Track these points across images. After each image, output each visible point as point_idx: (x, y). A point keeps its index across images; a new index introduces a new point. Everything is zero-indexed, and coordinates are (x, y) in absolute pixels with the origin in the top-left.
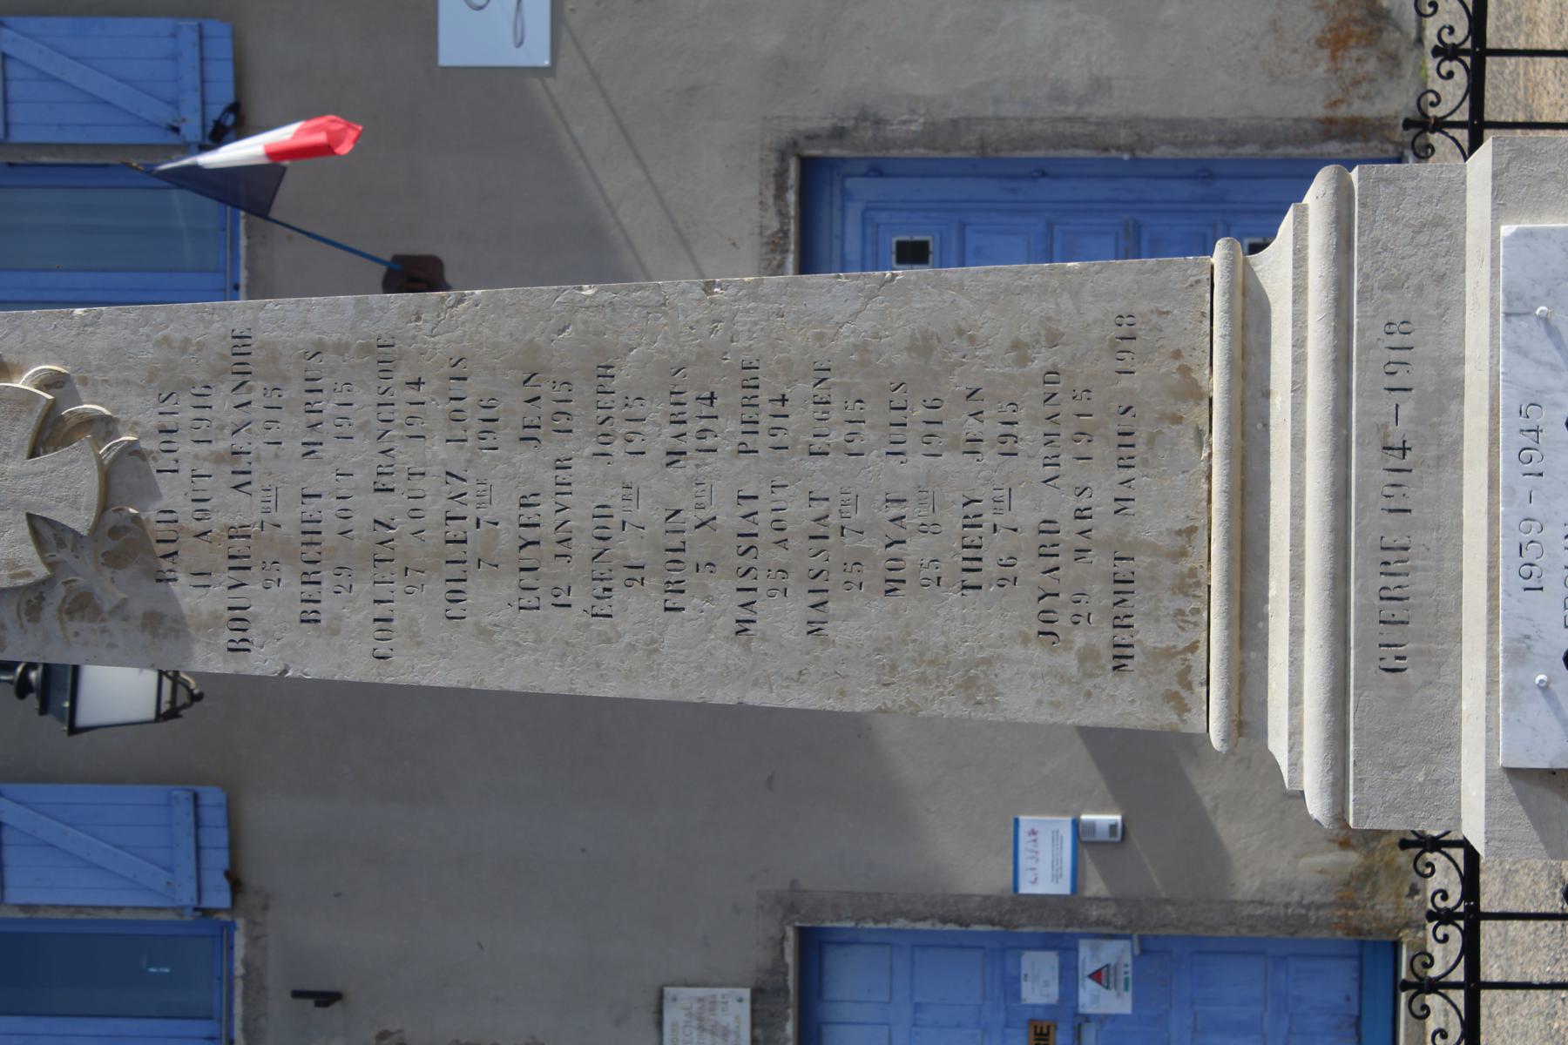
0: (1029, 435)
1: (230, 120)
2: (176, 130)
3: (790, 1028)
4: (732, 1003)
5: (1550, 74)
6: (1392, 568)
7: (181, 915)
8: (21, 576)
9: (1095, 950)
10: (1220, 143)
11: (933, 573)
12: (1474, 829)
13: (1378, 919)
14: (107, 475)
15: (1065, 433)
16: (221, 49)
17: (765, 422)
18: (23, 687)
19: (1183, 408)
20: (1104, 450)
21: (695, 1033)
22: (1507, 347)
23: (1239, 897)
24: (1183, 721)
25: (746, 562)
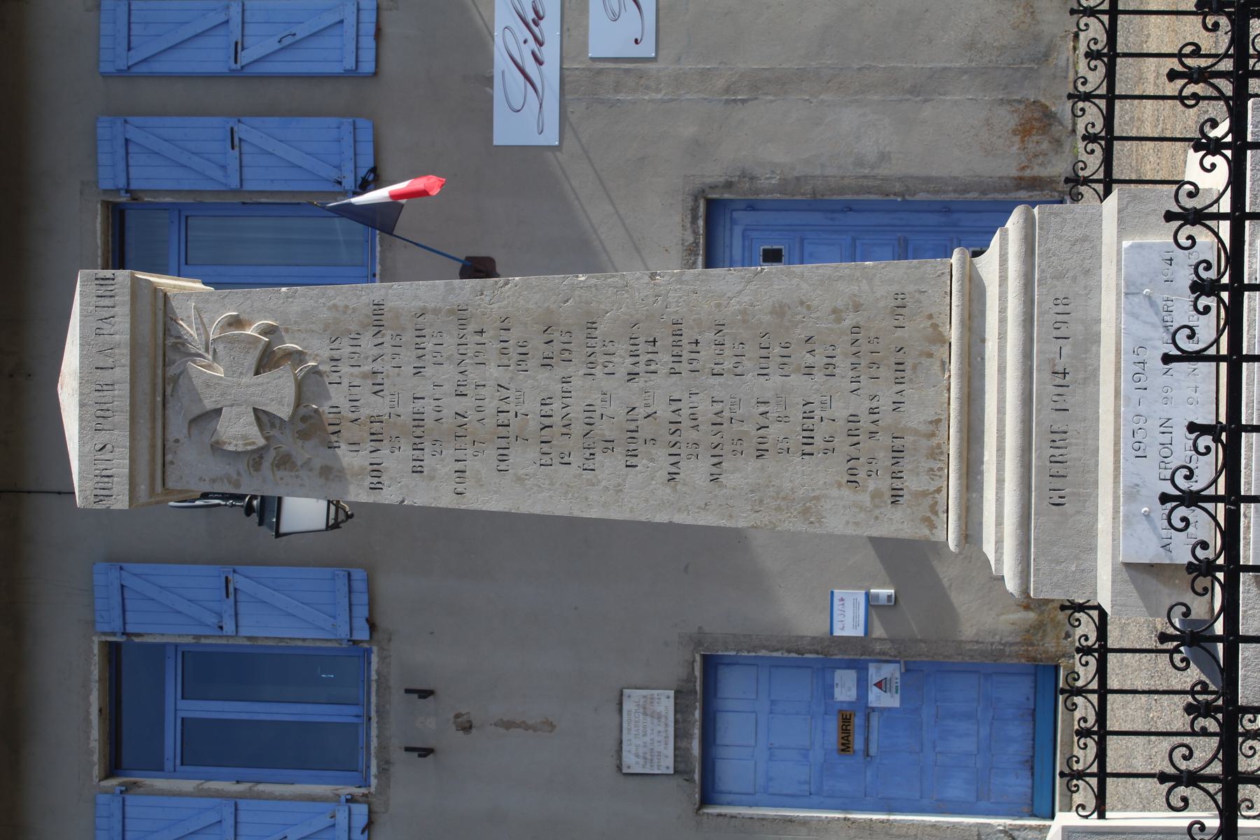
0: (843, 364)
1: (371, 177)
2: (340, 183)
3: (697, 714)
4: (664, 700)
5: (1151, 151)
6: (1058, 444)
7: (341, 644)
8: (250, 444)
9: (878, 669)
10: (955, 191)
11: (785, 446)
12: (1105, 600)
13: (1046, 652)
14: (300, 385)
15: (864, 363)
16: (366, 136)
17: (686, 356)
18: (249, 510)
19: (934, 348)
20: (886, 373)
21: (641, 717)
22: (1126, 313)
23: (963, 638)
24: (933, 534)
25: (674, 438)
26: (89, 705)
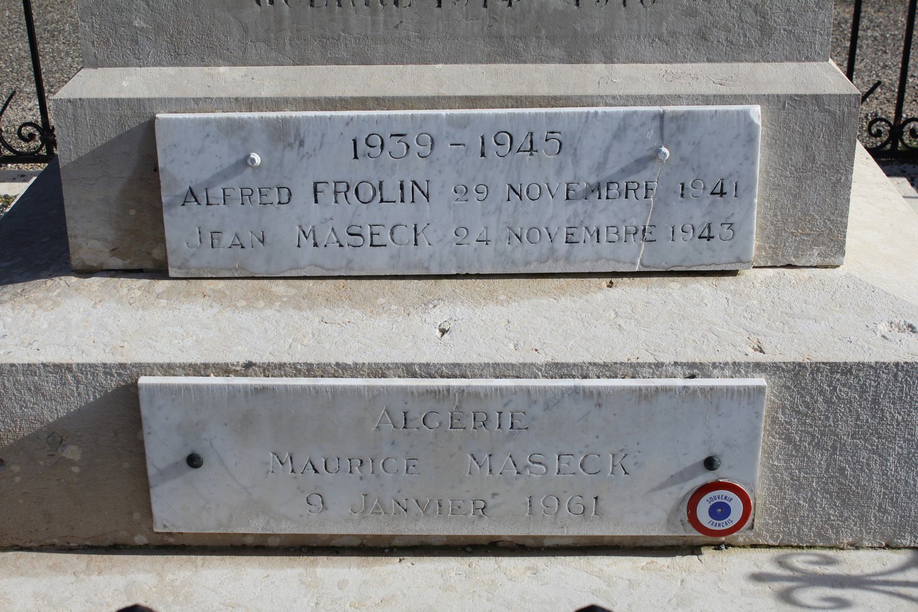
22: (627, 116)
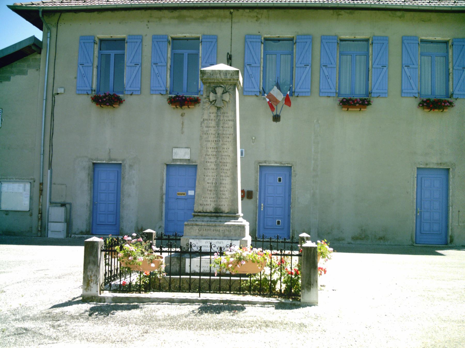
3: (185, 164)
26: (187, 34)
